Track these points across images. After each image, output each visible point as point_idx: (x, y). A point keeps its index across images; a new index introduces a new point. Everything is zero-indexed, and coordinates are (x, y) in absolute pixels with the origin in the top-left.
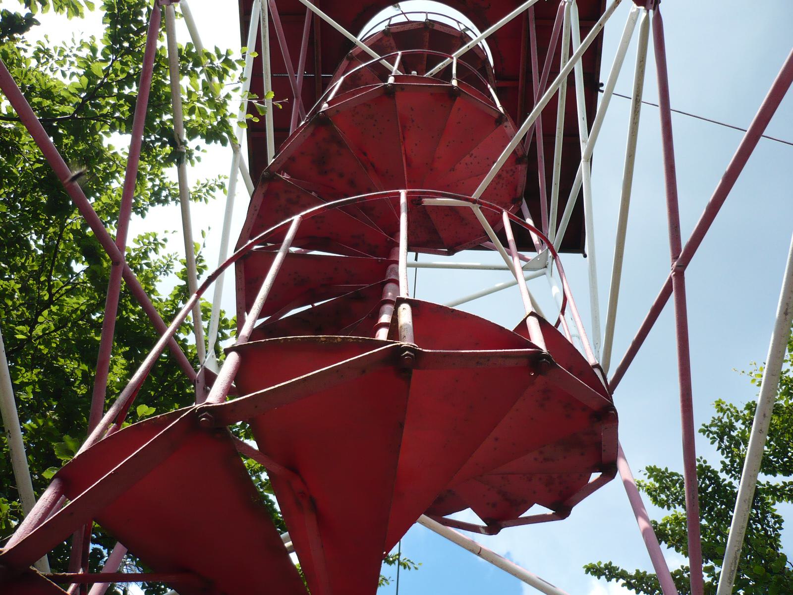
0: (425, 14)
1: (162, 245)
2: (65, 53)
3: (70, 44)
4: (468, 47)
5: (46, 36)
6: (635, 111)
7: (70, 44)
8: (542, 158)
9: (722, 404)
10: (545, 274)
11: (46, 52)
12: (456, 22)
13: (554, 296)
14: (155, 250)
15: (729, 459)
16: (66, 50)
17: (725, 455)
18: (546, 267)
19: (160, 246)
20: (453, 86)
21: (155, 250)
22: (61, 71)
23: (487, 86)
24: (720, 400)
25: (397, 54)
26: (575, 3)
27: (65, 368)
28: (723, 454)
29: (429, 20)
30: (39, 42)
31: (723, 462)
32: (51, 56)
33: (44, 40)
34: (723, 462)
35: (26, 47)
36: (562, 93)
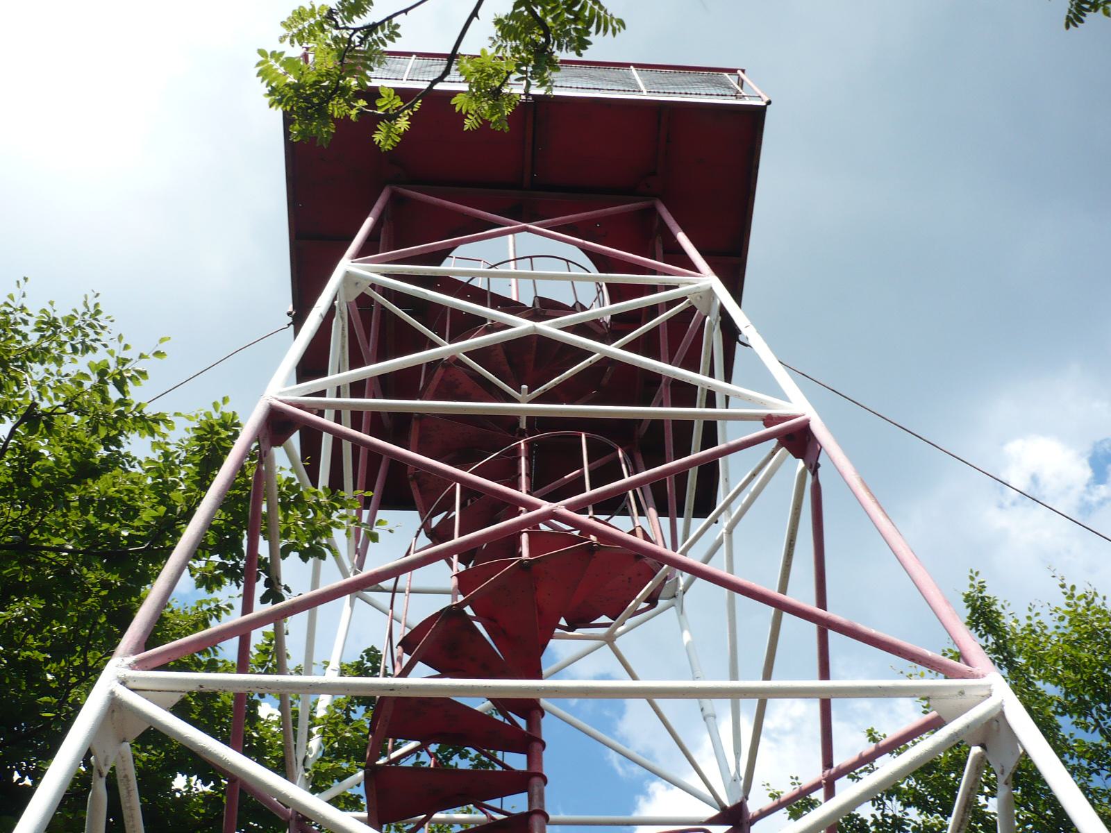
0: (529, 259)
1: (226, 611)
2: (76, 323)
3: (81, 309)
4: (591, 362)
5: (51, 303)
6: (788, 555)
7: (81, 309)
8: (671, 455)
9: (875, 733)
10: (674, 606)
11: (53, 323)
12: (565, 262)
13: (685, 644)
14: (218, 617)
15: (881, 811)
16: (76, 318)
17: (876, 807)
18: (675, 596)
19: (223, 612)
20: (592, 543)
21: (218, 617)
22: (71, 344)
23: (617, 450)
24: (873, 729)
25: (520, 444)
26: (718, 331)
27: (78, 701)
28: (874, 805)
29: (539, 297)
30: (44, 311)
31: (873, 816)
32: (60, 327)
33: (49, 309)
34: (873, 816)
35: (27, 318)
36: (701, 400)
